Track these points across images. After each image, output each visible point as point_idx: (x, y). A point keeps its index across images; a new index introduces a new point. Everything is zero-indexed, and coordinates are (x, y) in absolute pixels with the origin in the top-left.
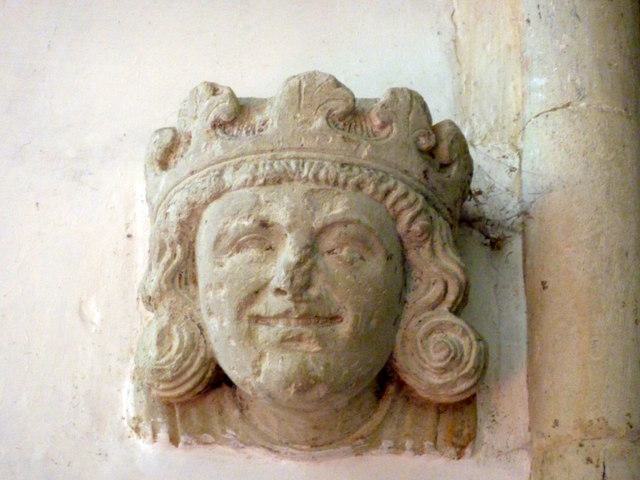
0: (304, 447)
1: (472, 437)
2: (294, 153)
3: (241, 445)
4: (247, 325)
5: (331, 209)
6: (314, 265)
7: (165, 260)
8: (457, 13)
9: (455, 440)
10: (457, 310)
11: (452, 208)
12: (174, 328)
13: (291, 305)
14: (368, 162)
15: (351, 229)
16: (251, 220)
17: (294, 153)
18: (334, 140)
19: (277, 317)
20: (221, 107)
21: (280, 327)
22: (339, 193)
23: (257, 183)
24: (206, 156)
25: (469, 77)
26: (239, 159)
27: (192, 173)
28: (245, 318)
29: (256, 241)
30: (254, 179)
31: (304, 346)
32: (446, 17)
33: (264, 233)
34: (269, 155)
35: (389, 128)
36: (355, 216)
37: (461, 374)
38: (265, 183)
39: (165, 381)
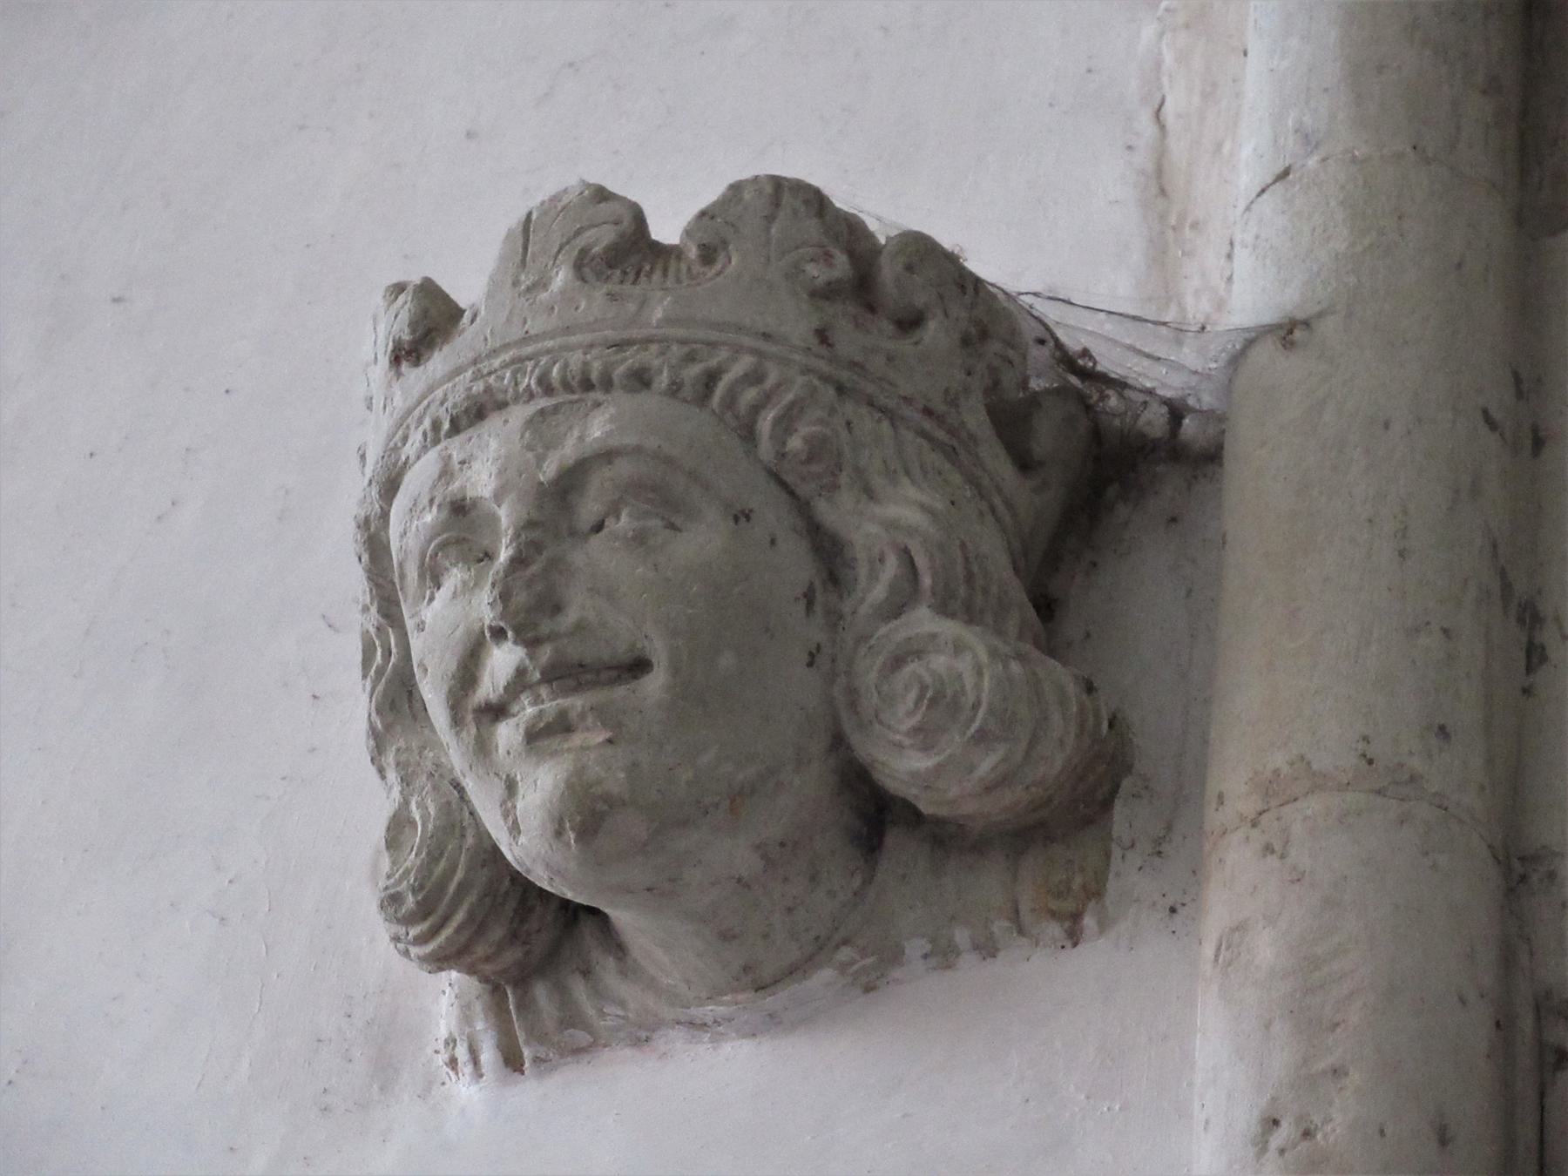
1: (1095, 892)
3: (643, 1034)
4: (473, 731)
6: (554, 564)
9: (1054, 905)
12: (413, 806)
14: (662, 331)
15: (624, 469)
16: (435, 509)
22: (597, 405)
25: (1182, 217)
28: (470, 717)
29: (453, 551)
30: (436, 425)
31: (577, 739)
36: (630, 440)
39: (409, 920)
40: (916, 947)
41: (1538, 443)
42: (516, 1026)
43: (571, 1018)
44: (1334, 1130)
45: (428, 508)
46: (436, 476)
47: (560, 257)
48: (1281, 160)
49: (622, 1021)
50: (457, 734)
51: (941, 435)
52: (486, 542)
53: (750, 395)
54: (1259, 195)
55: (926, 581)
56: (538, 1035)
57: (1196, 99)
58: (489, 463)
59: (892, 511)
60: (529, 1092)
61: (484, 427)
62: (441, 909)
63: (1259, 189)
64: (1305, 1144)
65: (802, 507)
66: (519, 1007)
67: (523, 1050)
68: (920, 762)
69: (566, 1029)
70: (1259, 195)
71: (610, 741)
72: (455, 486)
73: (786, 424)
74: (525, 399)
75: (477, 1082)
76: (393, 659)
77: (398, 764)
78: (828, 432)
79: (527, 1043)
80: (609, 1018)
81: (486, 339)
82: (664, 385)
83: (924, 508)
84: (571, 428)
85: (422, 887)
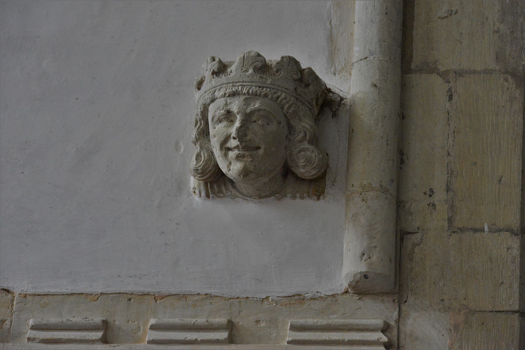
1: (323, 192)
2: (240, 84)
3: (234, 197)
4: (224, 151)
5: (254, 105)
7: (197, 126)
8: (332, 21)
10: (311, 142)
11: (310, 102)
12: (202, 153)
13: (238, 143)
16: (224, 111)
17: (240, 84)
18: (257, 78)
19: (235, 148)
20: (215, 66)
21: (236, 152)
22: (257, 99)
24: (209, 86)
25: (335, 47)
27: (205, 92)
30: (225, 94)
31: (245, 159)
32: (328, 23)
33: (229, 116)
34: (231, 84)
35: (280, 72)
36: (264, 108)
37: (312, 167)
38: (229, 96)
39: (199, 174)
40: (289, 195)
41: (403, 118)
42: (209, 190)
43: (220, 191)
44: (374, 258)
46: (224, 104)
47: (251, 66)
48: (366, 55)
49: (230, 194)
50: (221, 151)
51: (310, 107)
52: (232, 119)
53: (284, 101)
54: (360, 60)
55: (308, 138)
56: (213, 193)
57: (338, 22)
58: (236, 106)
59: (304, 124)
60: (210, 203)
62: (205, 173)
63: (360, 59)
64: (369, 260)
65: (288, 121)
66: (211, 187)
67: (210, 195)
68: (303, 170)
70: (360, 60)
71: (252, 161)
72: (228, 107)
73: (289, 108)
74: (244, 94)
78: (296, 109)
79: (211, 194)
81: (235, 79)
82: (270, 98)
83: (310, 125)
84: (252, 102)
85: (203, 169)
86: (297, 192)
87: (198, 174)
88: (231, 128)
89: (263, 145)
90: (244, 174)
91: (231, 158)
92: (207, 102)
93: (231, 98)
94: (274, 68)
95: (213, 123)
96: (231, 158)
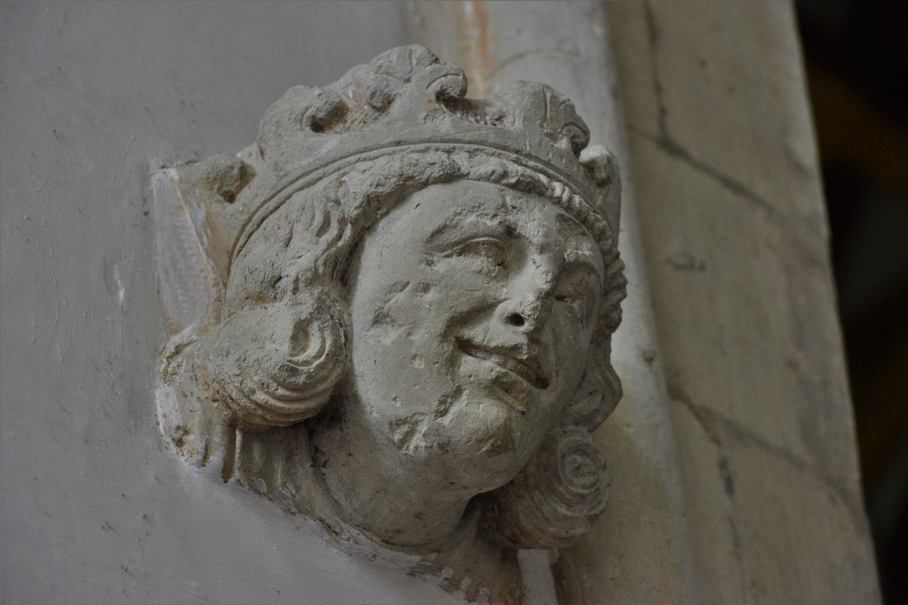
0: (375, 538)
3: (294, 510)
16: (496, 222)
23: (504, 181)
26: (476, 147)
27: (398, 143)
43: (266, 473)
45: (490, 217)
50: (442, 342)
61: (518, 193)
69: (261, 477)
75: (198, 467)
76: (340, 244)
77: (319, 298)
80: (286, 489)
86: (468, 571)
87: (283, 387)
88: (499, 285)
89: (560, 379)
90: (499, 443)
91: (470, 376)
92: (422, 173)
93: (519, 194)
94: (603, 169)
95: (429, 245)
96: (470, 376)
